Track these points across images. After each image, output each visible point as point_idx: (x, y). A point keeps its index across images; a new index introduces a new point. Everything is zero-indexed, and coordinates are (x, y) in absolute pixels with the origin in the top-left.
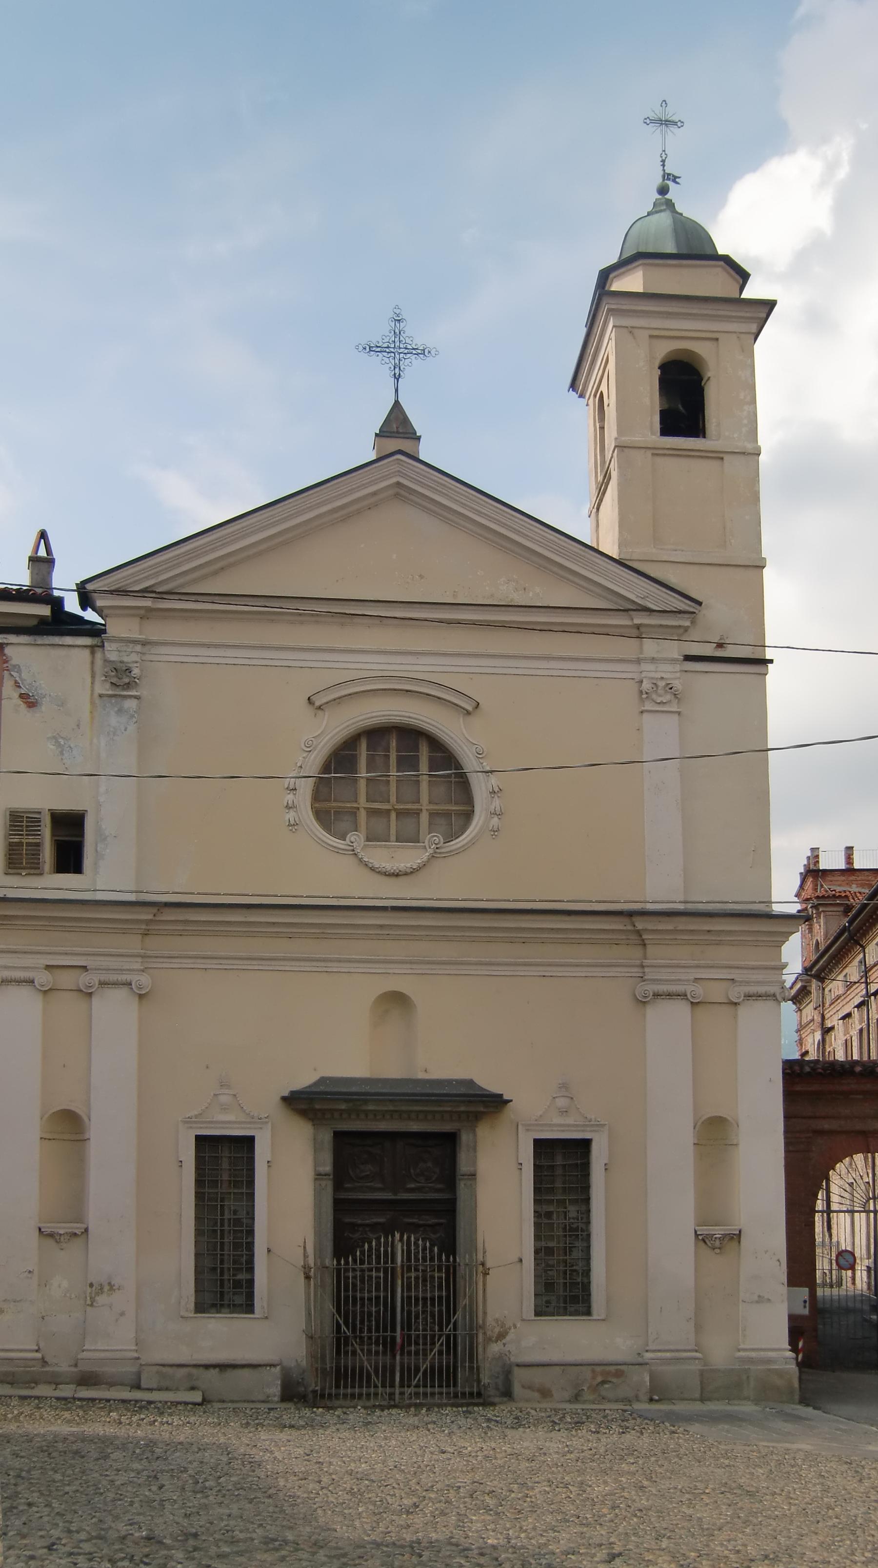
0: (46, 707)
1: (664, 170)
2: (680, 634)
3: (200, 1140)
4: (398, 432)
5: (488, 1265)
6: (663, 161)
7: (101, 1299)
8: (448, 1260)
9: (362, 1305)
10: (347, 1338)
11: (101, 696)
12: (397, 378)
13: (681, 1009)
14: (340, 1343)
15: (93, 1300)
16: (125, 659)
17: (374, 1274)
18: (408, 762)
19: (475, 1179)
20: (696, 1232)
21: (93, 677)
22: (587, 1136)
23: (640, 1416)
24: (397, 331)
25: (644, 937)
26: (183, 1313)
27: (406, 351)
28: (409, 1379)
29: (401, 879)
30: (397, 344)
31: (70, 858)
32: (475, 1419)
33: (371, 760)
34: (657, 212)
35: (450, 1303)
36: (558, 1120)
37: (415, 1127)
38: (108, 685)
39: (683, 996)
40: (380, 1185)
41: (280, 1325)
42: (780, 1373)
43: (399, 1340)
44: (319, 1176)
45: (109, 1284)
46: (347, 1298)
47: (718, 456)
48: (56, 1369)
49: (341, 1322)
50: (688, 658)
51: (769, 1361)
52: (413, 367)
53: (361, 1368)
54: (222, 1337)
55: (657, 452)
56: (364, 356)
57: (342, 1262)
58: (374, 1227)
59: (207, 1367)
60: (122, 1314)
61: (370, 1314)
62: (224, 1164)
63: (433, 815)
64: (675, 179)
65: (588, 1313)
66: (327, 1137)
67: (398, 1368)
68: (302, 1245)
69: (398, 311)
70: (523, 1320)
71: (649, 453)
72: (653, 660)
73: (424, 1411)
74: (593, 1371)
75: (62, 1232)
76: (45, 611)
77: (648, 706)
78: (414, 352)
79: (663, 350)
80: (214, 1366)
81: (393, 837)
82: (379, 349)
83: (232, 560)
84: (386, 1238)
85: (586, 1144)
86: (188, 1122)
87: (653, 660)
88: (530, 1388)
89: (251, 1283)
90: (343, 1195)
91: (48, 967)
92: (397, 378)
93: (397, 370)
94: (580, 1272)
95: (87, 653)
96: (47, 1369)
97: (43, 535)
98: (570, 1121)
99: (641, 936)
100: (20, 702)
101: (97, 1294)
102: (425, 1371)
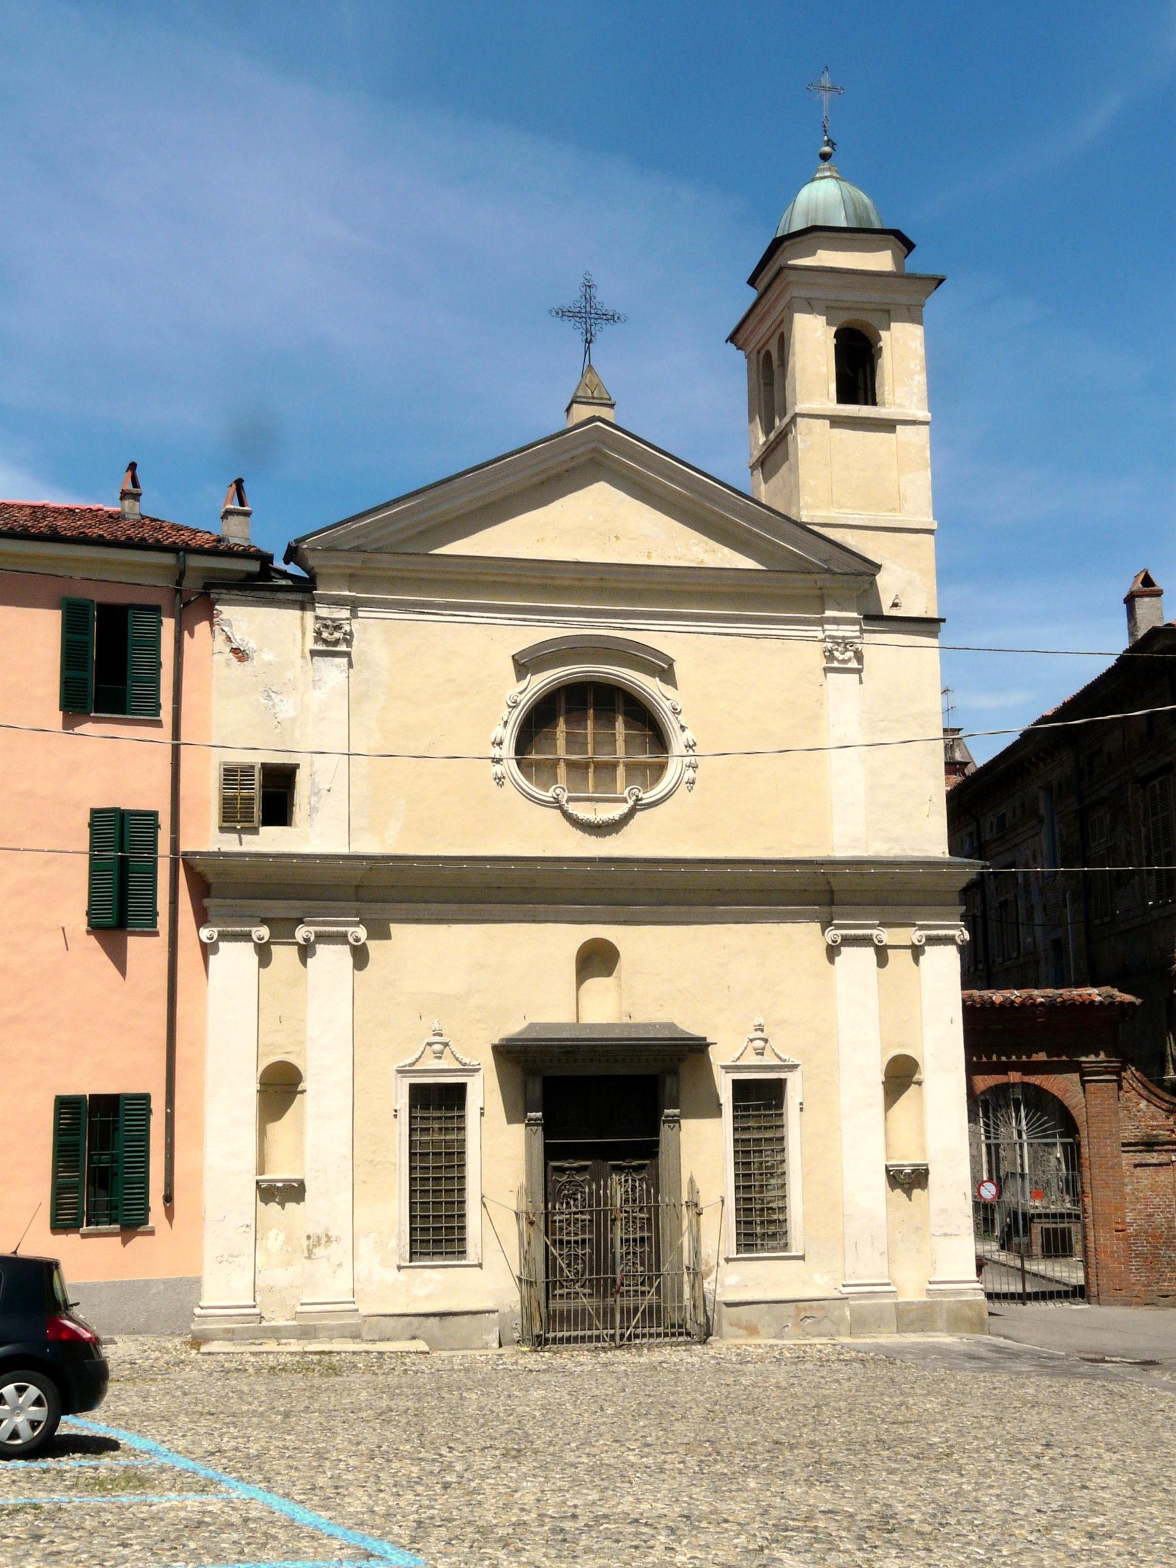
5: (701, 1205)
7: (319, 1252)
12: (588, 342)
15: (310, 1252)
21: (304, 634)
28: (629, 1321)
41: (492, 1270)
42: (969, 1304)
45: (327, 1235)
47: (888, 425)
48: (273, 1323)
51: (959, 1292)
53: (583, 1310)
54: (436, 1286)
55: (837, 422)
59: (427, 1315)
60: (340, 1265)
62: (436, 1103)
63: (628, 766)
67: (618, 1310)
73: (646, 1351)
74: (797, 1307)
76: (254, 567)
86: (401, 1072)
88: (738, 1325)
92: (588, 342)
96: (264, 1324)
98: (443, 1064)
100: (231, 655)
101: (315, 1246)
102: (644, 1312)
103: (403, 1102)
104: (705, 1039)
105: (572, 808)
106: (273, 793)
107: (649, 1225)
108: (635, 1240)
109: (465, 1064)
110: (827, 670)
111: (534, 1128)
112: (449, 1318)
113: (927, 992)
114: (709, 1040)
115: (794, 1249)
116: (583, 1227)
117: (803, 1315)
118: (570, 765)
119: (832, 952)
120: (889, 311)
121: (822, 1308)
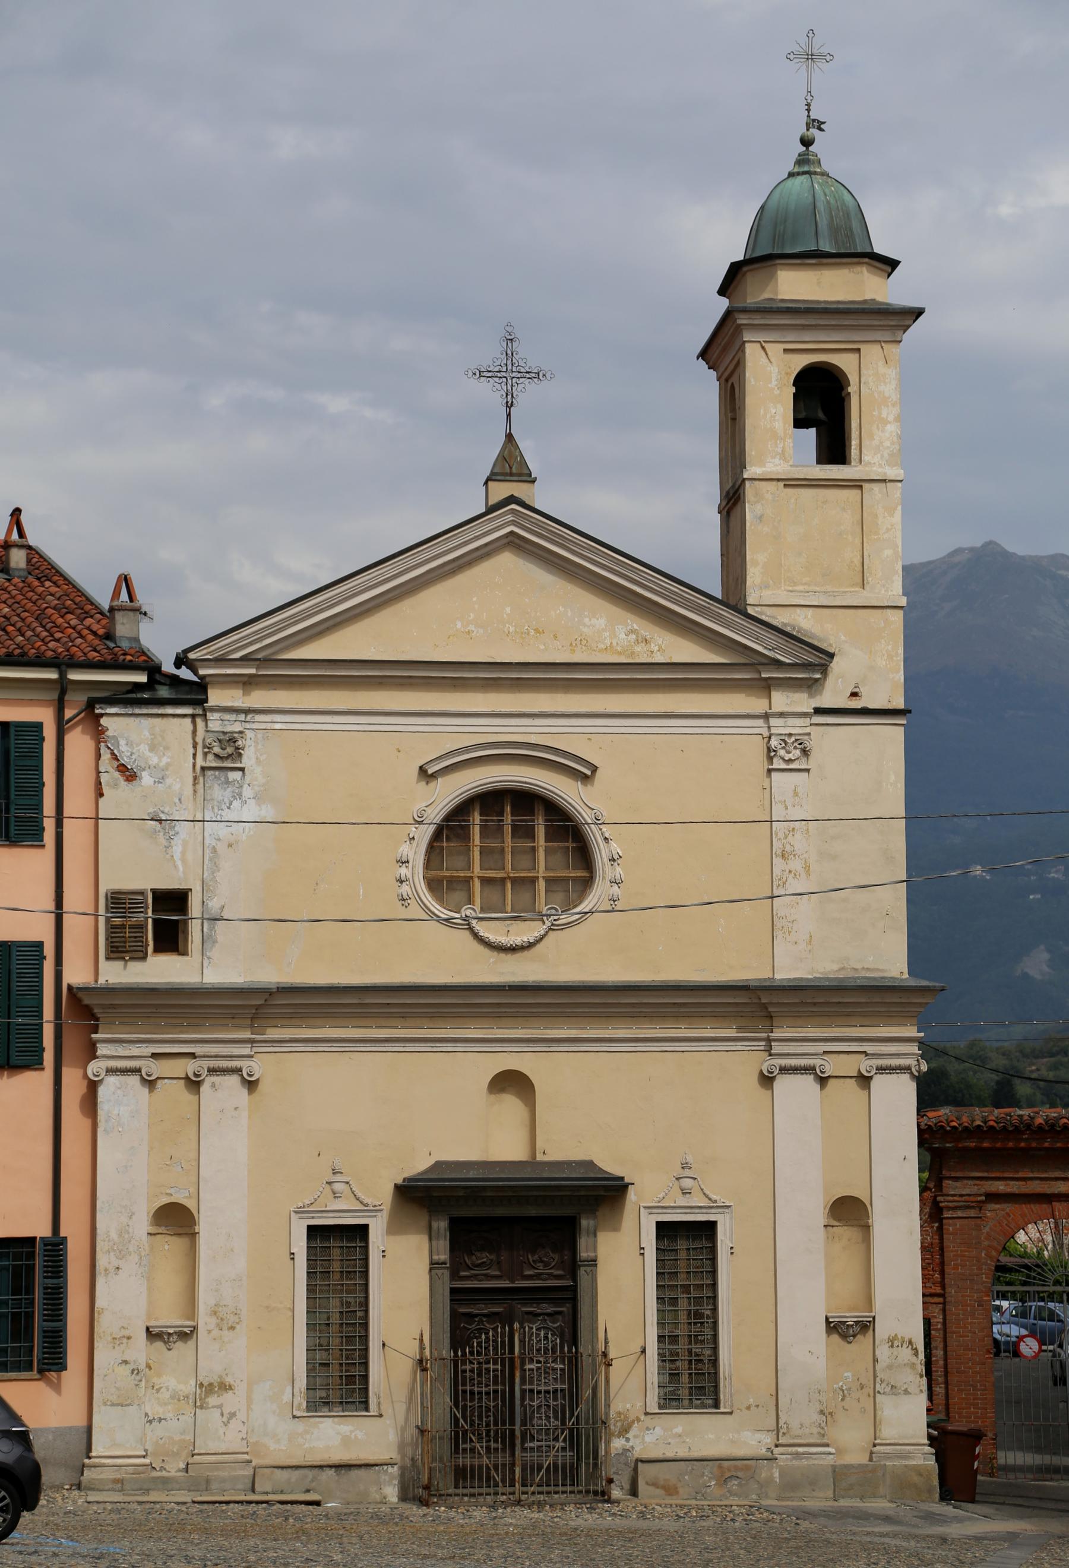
0: (146, 779)
1: (809, 116)
2: (812, 686)
3: (313, 1231)
4: (511, 474)
6: (808, 105)
7: (212, 1400)
8: (570, 1351)
9: (480, 1399)
10: (465, 1432)
11: (203, 769)
12: (509, 406)
13: (808, 1082)
14: (458, 1437)
16: (229, 729)
17: (491, 1366)
18: (524, 832)
19: (596, 1265)
20: (827, 1318)
22: (712, 1218)
23: (767, 1511)
24: (509, 352)
25: (770, 1010)
26: (298, 1414)
27: (519, 375)
29: (518, 955)
30: (510, 367)
31: (170, 938)
32: (600, 1514)
33: (484, 828)
34: (798, 174)
35: (573, 1396)
36: (682, 1201)
37: (533, 1211)
38: (210, 757)
39: (809, 1070)
40: (497, 1273)
42: (918, 1470)
43: (518, 1433)
44: (434, 1265)
46: (464, 1392)
49: (459, 1416)
50: (818, 711)
52: (527, 394)
54: (334, 1436)
56: (474, 382)
57: (460, 1353)
58: (491, 1316)
61: (488, 1409)
62: (337, 1250)
63: (549, 881)
64: (819, 125)
65: (365, 1405)
66: (442, 1225)
68: (418, 1337)
69: (509, 329)
70: (647, 1414)
71: (781, 484)
72: (782, 715)
74: (720, 1467)
75: (171, 1331)
77: (778, 764)
78: (528, 376)
79: (802, 361)
80: (330, 1467)
81: (509, 908)
82: (490, 374)
83: (338, 619)
84: (503, 1328)
85: (712, 1226)
87: (782, 715)
88: (655, 1485)
89: (365, 1378)
90: (12, 730)
91: (154, 1056)
92: (509, 406)
93: (509, 397)
94: (706, 1362)
95: (188, 721)
97: (125, 579)
99: (767, 1008)
103: (300, 1244)
104: (622, 1178)
105: (481, 928)
106: (168, 918)
107: (464, 1378)
108: (488, 1393)
109: (716, 1201)
110: (769, 771)
111: (440, 1272)
112: (355, 1473)
113: (875, 1129)
114: (626, 1180)
115: (722, 1405)
116: (496, 1377)
117: (728, 1475)
118: (486, 881)
119: (767, 1080)
120: (859, 350)
121: (747, 1468)
